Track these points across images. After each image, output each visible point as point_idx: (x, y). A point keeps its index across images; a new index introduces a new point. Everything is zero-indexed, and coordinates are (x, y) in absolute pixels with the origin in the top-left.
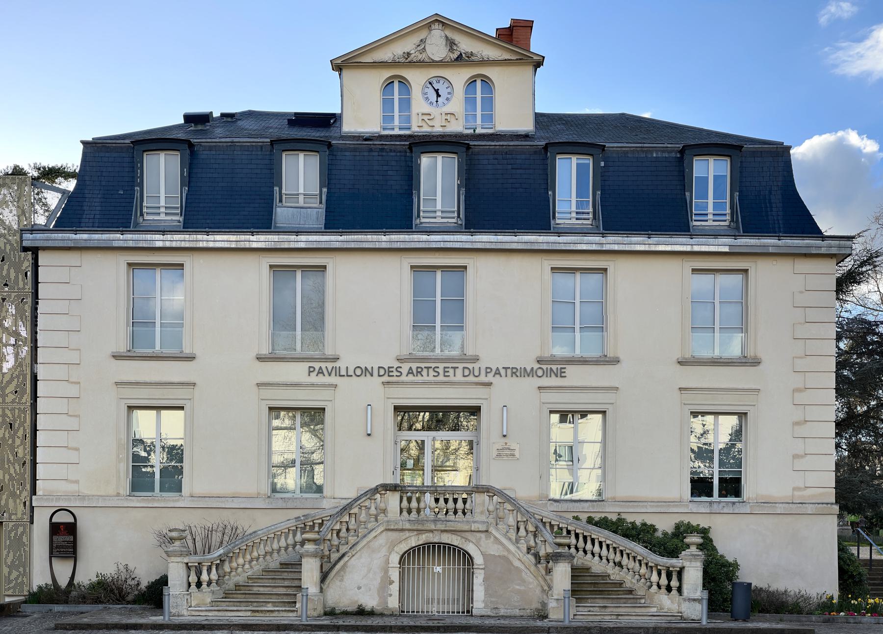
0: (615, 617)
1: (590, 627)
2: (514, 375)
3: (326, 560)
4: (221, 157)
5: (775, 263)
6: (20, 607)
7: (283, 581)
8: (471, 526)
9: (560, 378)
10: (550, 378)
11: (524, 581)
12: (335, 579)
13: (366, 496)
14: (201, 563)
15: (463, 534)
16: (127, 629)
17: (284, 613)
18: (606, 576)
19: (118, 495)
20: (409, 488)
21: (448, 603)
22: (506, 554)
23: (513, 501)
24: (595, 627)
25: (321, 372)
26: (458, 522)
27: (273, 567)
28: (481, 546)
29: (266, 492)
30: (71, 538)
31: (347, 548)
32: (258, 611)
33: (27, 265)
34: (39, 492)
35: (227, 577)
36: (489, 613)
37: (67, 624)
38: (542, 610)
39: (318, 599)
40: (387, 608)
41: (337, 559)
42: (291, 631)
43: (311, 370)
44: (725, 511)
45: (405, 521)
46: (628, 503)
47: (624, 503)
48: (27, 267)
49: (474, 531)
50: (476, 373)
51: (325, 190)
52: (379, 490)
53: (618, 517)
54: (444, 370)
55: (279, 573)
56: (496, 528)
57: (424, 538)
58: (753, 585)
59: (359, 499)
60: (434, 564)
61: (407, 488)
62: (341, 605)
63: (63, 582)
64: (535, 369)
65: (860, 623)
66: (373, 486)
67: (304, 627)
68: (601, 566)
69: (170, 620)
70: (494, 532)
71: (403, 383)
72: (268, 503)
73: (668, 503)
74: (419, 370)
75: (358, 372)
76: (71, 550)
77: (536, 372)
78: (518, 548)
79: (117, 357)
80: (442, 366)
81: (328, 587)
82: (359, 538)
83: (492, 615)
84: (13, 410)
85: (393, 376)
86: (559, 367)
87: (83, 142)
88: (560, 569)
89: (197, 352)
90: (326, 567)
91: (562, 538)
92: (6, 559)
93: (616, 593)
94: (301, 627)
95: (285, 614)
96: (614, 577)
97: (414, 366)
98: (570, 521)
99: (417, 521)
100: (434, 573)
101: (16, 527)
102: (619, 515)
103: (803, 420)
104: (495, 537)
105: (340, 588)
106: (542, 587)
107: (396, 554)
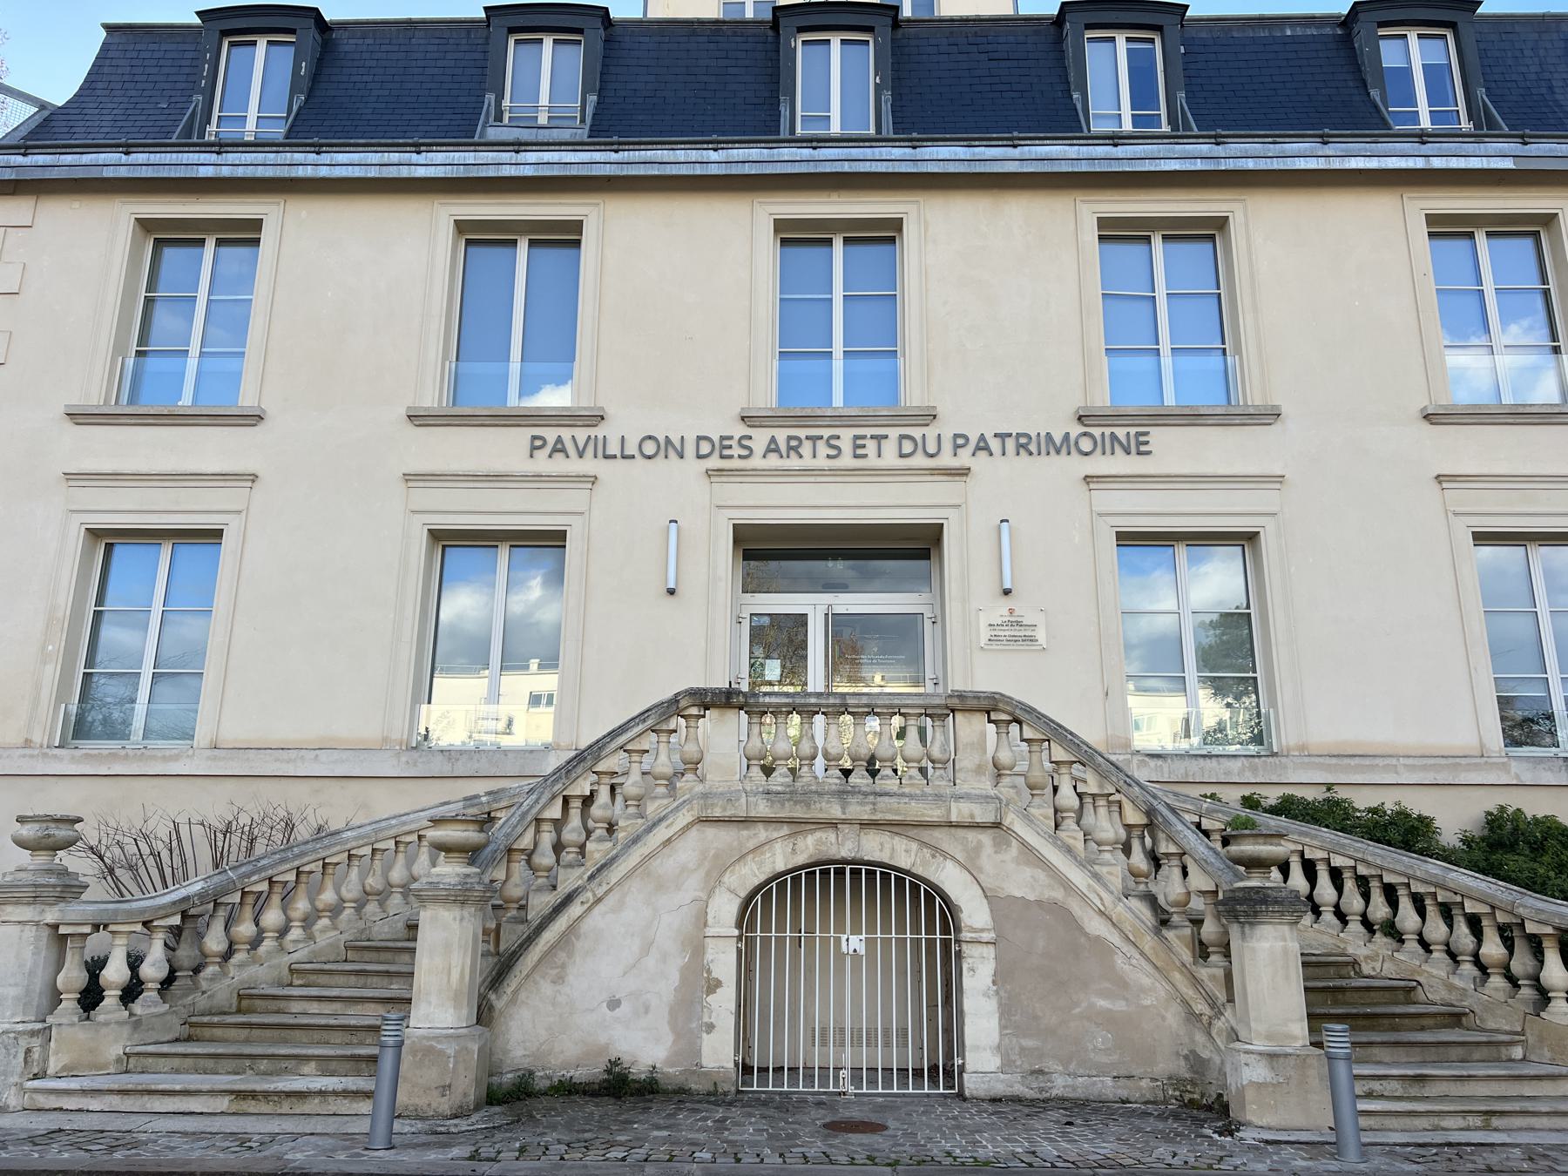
0: (1477, 1121)
2: (1022, 451)
3: (514, 912)
4: (384, 48)
7: (386, 981)
9: (1138, 457)
10: (1111, 457)
12: (536, 976)
13: (644, 721)
14: (152, 921)
15: (926, 835)
17: (340, 1100)
18: (1347, 964)
19: (28, 743)
20: (767, 700)
21: (887, 1044)
22: (1058, 894)
23: (1069, 736)
25: (559, 448)
26: (911, 796)
27: (383, 937)
28: (981, 870)
29: (405, 737)
31: (580, 877)
32: (252, 1095)
35: (210, 970)
36: (1019, 1089)
38: (1193, 1083)
39: (457, 1052)
40: (697, 1070)
41: (547, 911)
43: (536, 445)
45: (756, 794)
46: (1347, 761)
47: (1334, 761)
49: (958, 826)
52: (683, 703)
53: (1328, 795)
54: (854, 442)
56: (1024, 816)
57: (809, 847)
60: (840, 928)
61: (761, 700)
62: (554, 1061)
64: (1073, 436)
66: (668, 694)
68: (1323, 933)
70: (1020, 828)
71: (755, 472)
72: (408, 762)
73: (1451, 761)
74: (794, 443)
75: (649, 448)
77: (1077, 443)
78: (1096, 877)
79: (78, 417)
80: (847, 435)
81: (513, 1001)
83: (1030, 1094)
85: (731, 457)
86: (1133, 430)
87: (107, 27)
88: (1266, 945)
89: (269, 406)
90: (508, 941)
91: (1261, 840)
93: (1415, 1021)
95: (344, 1106)
96: (1374, 969)
97: (781, 435)
98: (1205, 805)
99: (791, 793)
100: (840, 956)
102: (1329, 790)
104: (1024, 843)
105: (553, 1005)
106: (1185, 1003)
107: (727, 896)
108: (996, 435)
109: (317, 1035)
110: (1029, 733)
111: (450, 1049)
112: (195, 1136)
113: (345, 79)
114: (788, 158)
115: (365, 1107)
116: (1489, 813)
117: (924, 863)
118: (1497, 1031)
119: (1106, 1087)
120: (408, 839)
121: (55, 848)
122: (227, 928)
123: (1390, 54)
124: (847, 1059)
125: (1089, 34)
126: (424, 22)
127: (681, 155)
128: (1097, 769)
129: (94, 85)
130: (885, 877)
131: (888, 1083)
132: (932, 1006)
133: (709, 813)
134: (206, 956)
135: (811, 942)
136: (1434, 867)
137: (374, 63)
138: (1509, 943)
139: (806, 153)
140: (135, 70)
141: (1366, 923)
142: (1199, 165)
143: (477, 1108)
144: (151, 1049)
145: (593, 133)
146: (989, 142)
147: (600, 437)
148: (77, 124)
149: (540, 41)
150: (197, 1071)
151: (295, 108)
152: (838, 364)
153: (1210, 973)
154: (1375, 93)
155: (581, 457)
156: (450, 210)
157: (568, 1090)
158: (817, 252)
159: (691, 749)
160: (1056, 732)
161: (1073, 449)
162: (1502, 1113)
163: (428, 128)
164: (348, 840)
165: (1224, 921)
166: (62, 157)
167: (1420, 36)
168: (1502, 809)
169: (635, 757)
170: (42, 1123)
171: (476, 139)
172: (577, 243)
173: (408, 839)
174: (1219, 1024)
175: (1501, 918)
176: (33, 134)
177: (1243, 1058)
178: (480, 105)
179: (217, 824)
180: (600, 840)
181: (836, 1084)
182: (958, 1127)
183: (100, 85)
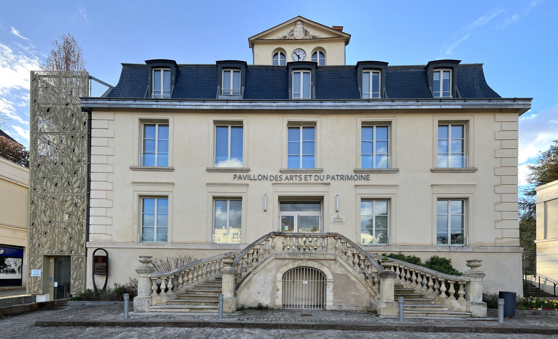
0: (425, 315)
1: (426, 327)
3: (239, 276)
4: (192, 73)
5: (484, 116)
6: (66, 303)
7: (214, 288)
8: (326, 257)
11: (358, 289)
12: (244, 288)
15: (321, 262)
16: (88, 326)
17: (210, 310)
18: (400, 286)
19: (133, 241)
20: (288, 234)
21: (311, 301)
22: (346, 273)
24: (431, 327)
25: (240, 178)
26: (318, 254)
30: (105, 264)
32: (193, 309)
33: (85, 118)
34: (91, 240)
35: (180, 286)
37: (44, 322)
40: (275, 305)
41: (245, 276)
42: (208, 327)
44: (458, 250)
46: (404, 247)
47: (402, 247)
48: (85, 120)
50: (322, 179)
51: (243, 88)
52: (271, 235)
55: (213, 284)
57: (297, 264)
58: (517, 295)
59: (259, 240)
63: (101, 286)
65: (554, 315)
66: (268, 233)
67: (218, 324)
69: (128, 317)
70: (339, 260)
74: (291, 177)
75: (260, 178)
76: (104, 271)
77: (354, 177)
78: (354, 269)
79: (133, 169)
80: (303, 175)
81: (240, 292)
82: (259, 264)
83: (338, 309)
84: (68, 191)
85: (278, 180)
86: (366, 174)
87: (123, 64)
89: (175, 167)
90: (238, 281)
92: (73, 275)
94: (216, 324)
95: (211, 311)
97: (289, 175)
100: (303, 285)
101: (78, 258)
103: (500, 201)
104: (340, 263)
105: (247, 293)
106: (370, 293)
108: (336, 175)
109: (203, 298)
110: (342, 241)
111: (231, 301)
112: (185, 316)
113: (183, 81)
114: (291, 105)
115: (217, 311)
116: (432, 257)
117: (320, 267)
118: (429, 299)
119: (353, 308)
120: (214, 261)
121: (148, 263)
122: (182, 278)
123: (436, 77)
124: (304, 303)
125: (364, 71)
126: (201, 65)
127: (266, 104)
128: (356, 248)
129: (122, 81)
130: (312, 270)
131: (311, 308)
132: (317, 294)
133: (277, 257)
134: (179, 283)
135: (297, 282)
136: (421, 268)
137: (190, 77)
138: (434, 282)
139: (295, 104)
140: (132, 77)
141: (405, 278)
142: (388, 108)
143: (236, 312)
144: (172, 300)
145: (244, 98)
146: (339, 101)
147: (249, 175)
148: (120, 92)
149: (230, 71)
150: (181, 305)
151: (172, 89)
152: (301, 158)
153: (375, 288)
154: (430, 88)
155: (245, 179)
156: (360, 119)
157: (251, 308)
158: (296, 130)
159: (273, 244)
160: (348, 241)
161: (353, 179)
162: (430, 313)
163: (205, 96)
164: (203, 262)
165: (379, 278)
166: (119, 102)
167: (444, 71)
168: (435, 256)
169: (262, 246)
170: (155, 314)
171: (216, 99)
172: (242, 127)
173: (214, 261)
174: (376, 297)
175: (434, 277)
176: (109, 95)
177: (381, 303)
178: (216, 91)
179: (175, 258)
180: (255, 262)
181: (301, 308)
182: (326, 315)
183: (124, 81)
